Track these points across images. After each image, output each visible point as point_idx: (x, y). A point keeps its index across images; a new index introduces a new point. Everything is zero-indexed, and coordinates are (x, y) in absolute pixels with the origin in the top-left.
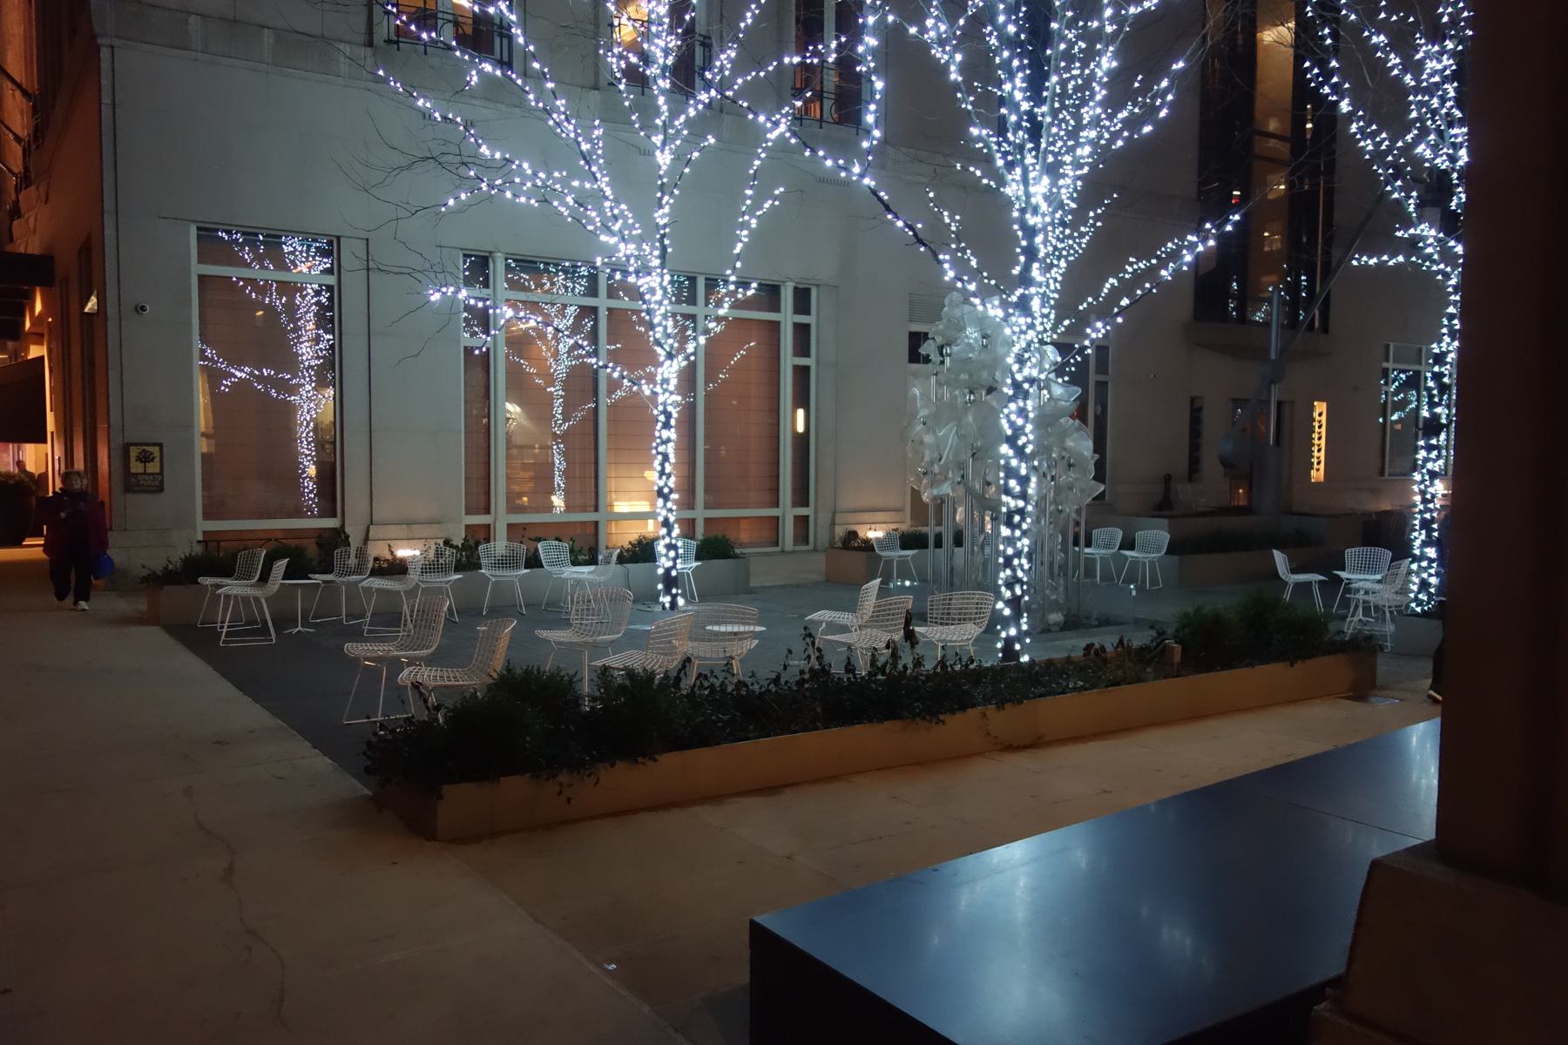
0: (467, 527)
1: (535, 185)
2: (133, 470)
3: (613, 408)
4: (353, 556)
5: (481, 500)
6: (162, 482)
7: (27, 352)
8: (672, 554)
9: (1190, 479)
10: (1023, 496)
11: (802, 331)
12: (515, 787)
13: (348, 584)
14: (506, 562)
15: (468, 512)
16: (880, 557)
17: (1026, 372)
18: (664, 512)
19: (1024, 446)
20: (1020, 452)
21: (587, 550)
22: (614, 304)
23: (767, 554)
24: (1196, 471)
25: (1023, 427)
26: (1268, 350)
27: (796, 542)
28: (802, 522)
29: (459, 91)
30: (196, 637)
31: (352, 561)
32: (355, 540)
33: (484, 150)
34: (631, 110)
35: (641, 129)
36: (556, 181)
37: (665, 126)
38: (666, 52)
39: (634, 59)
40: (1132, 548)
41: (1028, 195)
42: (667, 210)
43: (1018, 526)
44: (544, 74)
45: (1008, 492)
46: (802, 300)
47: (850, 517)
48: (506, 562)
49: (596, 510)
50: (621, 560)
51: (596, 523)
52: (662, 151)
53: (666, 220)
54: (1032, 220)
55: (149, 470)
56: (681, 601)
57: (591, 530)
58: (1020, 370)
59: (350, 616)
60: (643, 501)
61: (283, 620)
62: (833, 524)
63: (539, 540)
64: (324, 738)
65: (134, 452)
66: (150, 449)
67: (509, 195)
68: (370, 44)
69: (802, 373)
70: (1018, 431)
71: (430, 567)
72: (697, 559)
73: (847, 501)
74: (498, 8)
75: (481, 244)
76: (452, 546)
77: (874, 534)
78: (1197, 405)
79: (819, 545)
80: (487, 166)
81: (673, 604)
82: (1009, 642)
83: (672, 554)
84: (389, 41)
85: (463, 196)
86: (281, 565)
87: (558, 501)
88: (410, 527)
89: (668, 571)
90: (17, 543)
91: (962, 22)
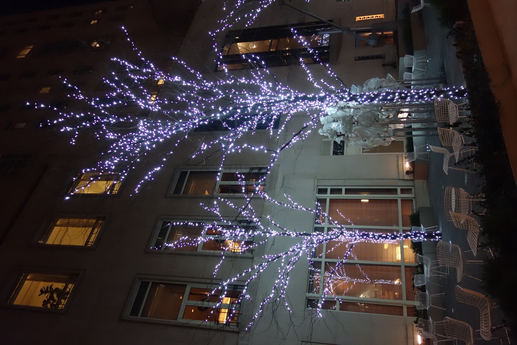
0: (408, 316)
1: (283, 279)
3: (360, 258)
5: (397, 310)
7: (47, 233)
9: (385, 58)
10: (394, 94)
11: (333, 191)
14: (423, 299)
17: (346, 96)
19: (374, 95)
20: (376, 96)
21: (419, 269)
22: (324, 257)
23: (416, 203)
24: (381, 56)
25: (367, 96)
26: (339, 34)
27: (411, 193)
28: (403, 191)
29: (253, 303)
33: (271, 296)
34: (259, 244)
35: (265, 241)
36: (282, 271)
37: (264, 232)
38: (241, 231)
39: (243, 243)
40: (411, 68)
41: (284, 100)
42: (291, 233)
43: (406, 94)
44: (246, 272)
45: (392, 100)
46: (322, 191)
47: (401, 174)
49: (400, 266)
50: (421, 254)
51: (405, 267)
52: (272, 234)
53: (295, 233)
54: (293, 98)
57: (408, 269)
58: (346, 98)
60: (397, 250)
62: (403, 180)
63: (414, 286)
67: (285, 287)
68: (238, 333)
69: (348, 191)
70: (369, 97)
71: (427, 329)
72: (420, 226)
73: (395, 176)
74: (225, 286)
75: (303, 302)
77: (407, 165)
78: (358, 59)
80: (277, 295)
81: (439, 235)
82: (455, 94)
84: (238, 326)
85: (287, 304)
87: (396, 282)
89: (425, 237)
91: (230, 128)
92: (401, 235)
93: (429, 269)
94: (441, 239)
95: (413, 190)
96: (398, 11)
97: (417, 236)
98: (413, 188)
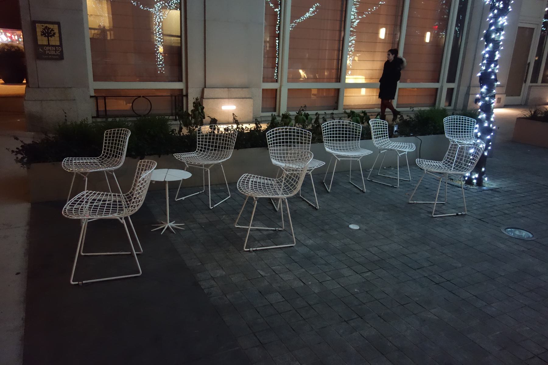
0: (263, 90)
2: (40, 43)
6: (62, 52)
28: (450, 91)
51: (338, 90)
55: (52, 43)
57: (332, 94)
65: (39, 28)
66: (51, 26)
88: (230, 89)
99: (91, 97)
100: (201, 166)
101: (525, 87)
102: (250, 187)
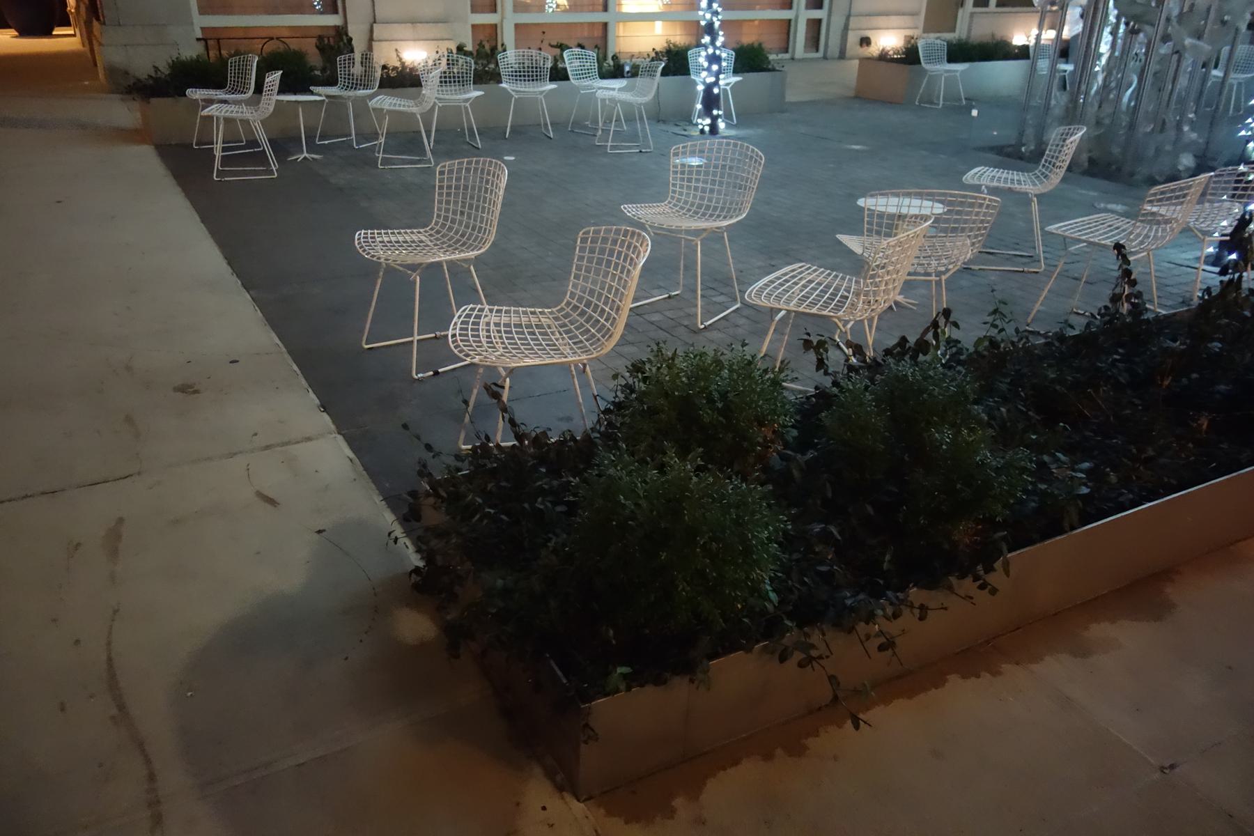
0: (473, 26)
4: (358, 64)
8: (715, 67)
12: (737, 673)
13: (356, 101)
15: (474, 9)
16: (926, 71)
18: (708, 16)
28: (815, 25)
30: (186, 161)
31: (357, 70)
32: (359, 45)
47: (864, 22)
48: (529, 73)
49: (605, 9)
51: (605, 25)
56: (721, 125)
57: (598, 33)
59: (362, 137)
61: (284, 144)
62: (846, 28)
63: (562, 47)
64: (348, 382)
72: (736, 71)
76: (467, 54)
79: (829, 54)
83: (715, 67)
86: (274, 78)
90: (47, 33)
92: (716, 13)
93: (615, 94)
94: (702, 131)
95: (814, 55)
96: (831, 29)
97: (711, 63)
98: (820, 54)
99: (198, 39)
100: (680, 231)
101: (964, 14)
102: (484, 340)
